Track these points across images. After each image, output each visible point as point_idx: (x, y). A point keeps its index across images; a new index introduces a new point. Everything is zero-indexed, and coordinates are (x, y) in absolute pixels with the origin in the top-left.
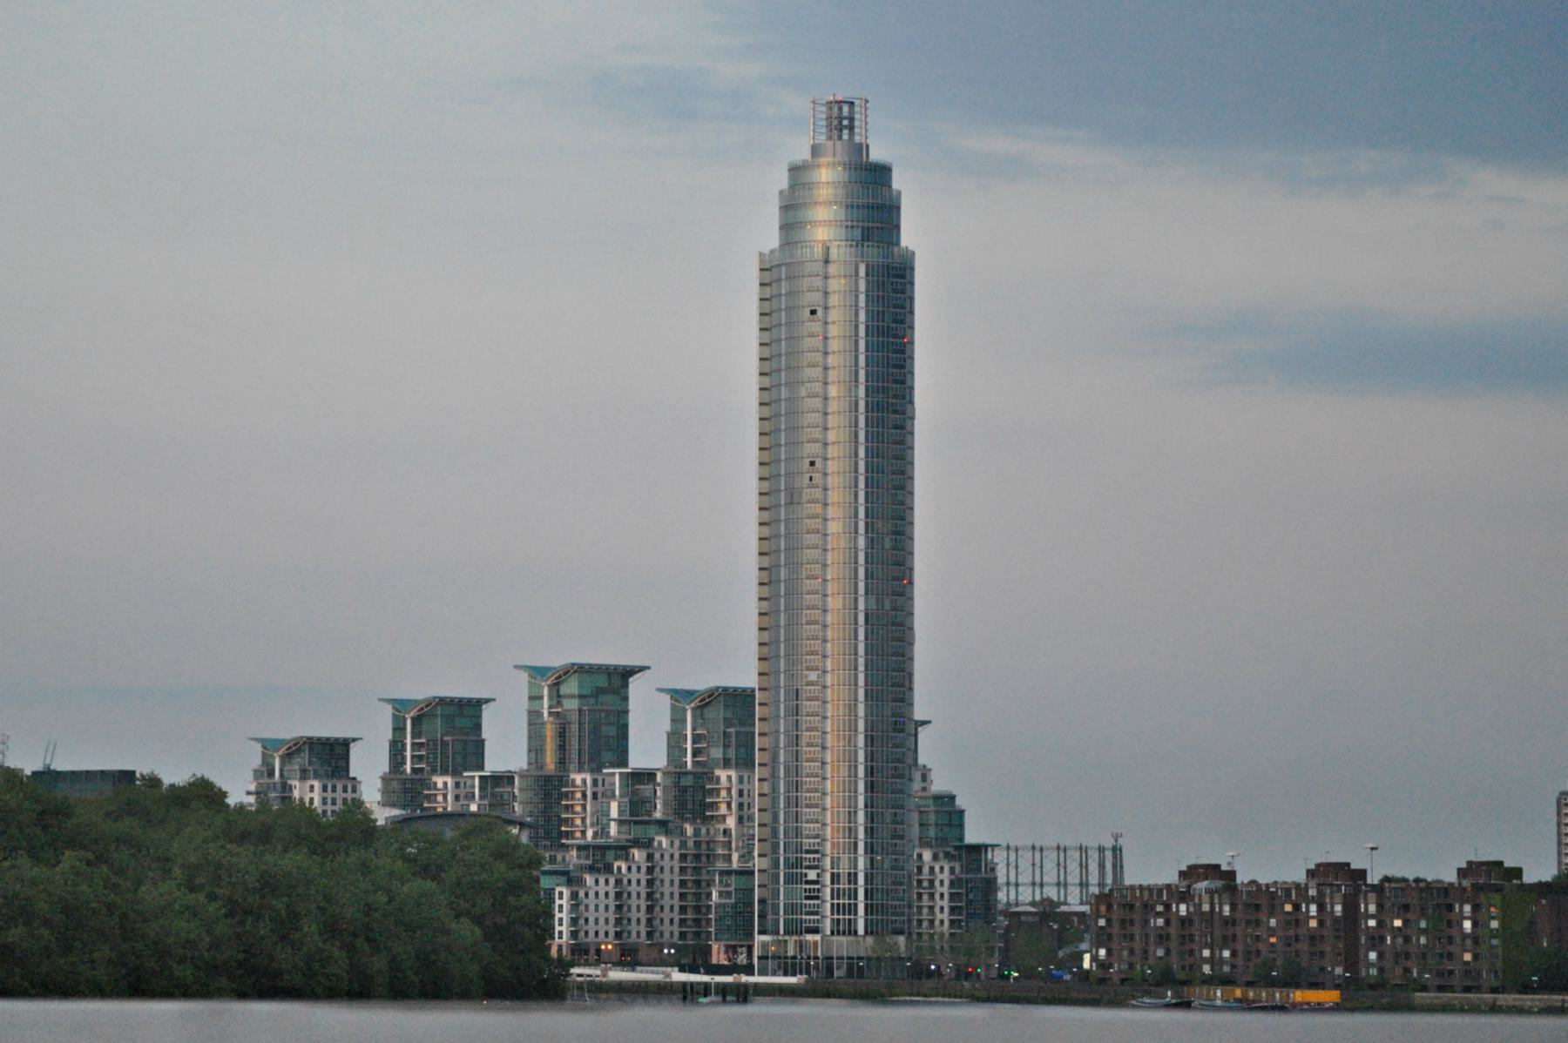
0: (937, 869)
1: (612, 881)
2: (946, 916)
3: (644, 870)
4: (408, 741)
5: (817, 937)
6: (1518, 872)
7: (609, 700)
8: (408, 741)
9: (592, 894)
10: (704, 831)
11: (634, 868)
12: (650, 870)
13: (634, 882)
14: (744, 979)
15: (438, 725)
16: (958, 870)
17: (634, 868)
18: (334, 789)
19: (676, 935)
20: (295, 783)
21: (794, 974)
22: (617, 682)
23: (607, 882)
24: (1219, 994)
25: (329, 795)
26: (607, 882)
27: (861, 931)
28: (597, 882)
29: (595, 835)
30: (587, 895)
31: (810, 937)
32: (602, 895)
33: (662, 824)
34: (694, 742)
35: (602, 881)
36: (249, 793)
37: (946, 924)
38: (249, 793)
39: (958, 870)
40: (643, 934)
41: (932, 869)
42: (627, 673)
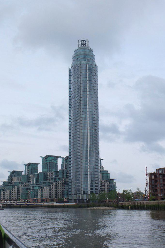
0: (105, 184)
2: (107, 190)
3: (55, 186)
5: (80, 195)
9: (45, 190)
10: (66, 180)
11: (53, 186)
13: (53, 188)
14: (66, 204)
17: (53, 186)
18: (19, 178)
20: (13, 177)
21: (74, 203)
22: (55, 158)
23: (48, 188)
24: (121, 202)
25: (18, 179)
26: (48, 188)
27: (89, 194)
28: (46, 188)
30: (44, 190)
31: (78, 195)
32: (47, 190)
34: (65, 165)
35: (47, 188)
36: (7, 179)
37: (107, 191)
38: (7, 179)
41: (104, 184)
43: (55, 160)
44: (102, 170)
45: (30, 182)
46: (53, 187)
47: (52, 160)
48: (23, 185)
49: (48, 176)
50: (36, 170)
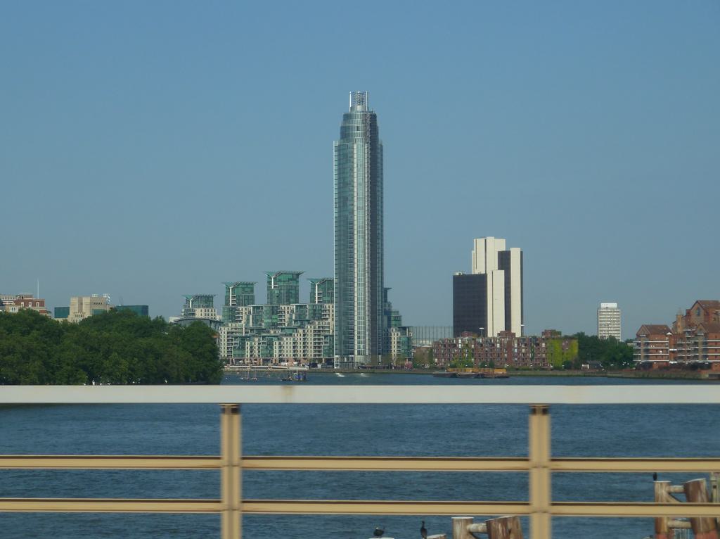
1: (292, 339)
3: (302, 335)
4: (317, 292)
6: (560, 333)
7: (293, 283)
8: (317, 292)
12: (304, 335)
15: (239, 290)
16: (399, 334)
19: (313, 355)
22: (295, 277)
25: (207, 312)
29: (288, 325)
33: (308, 321)
39: (399, 334)
40: (302, 355)
42: (298, 275)
43: (295, 280)
44: (387, 308)
45: (240, 321)
46: (299, 337)
47: (290, 279)
48: (226, 328)
49: (326, 311)
50: (23, 378)
